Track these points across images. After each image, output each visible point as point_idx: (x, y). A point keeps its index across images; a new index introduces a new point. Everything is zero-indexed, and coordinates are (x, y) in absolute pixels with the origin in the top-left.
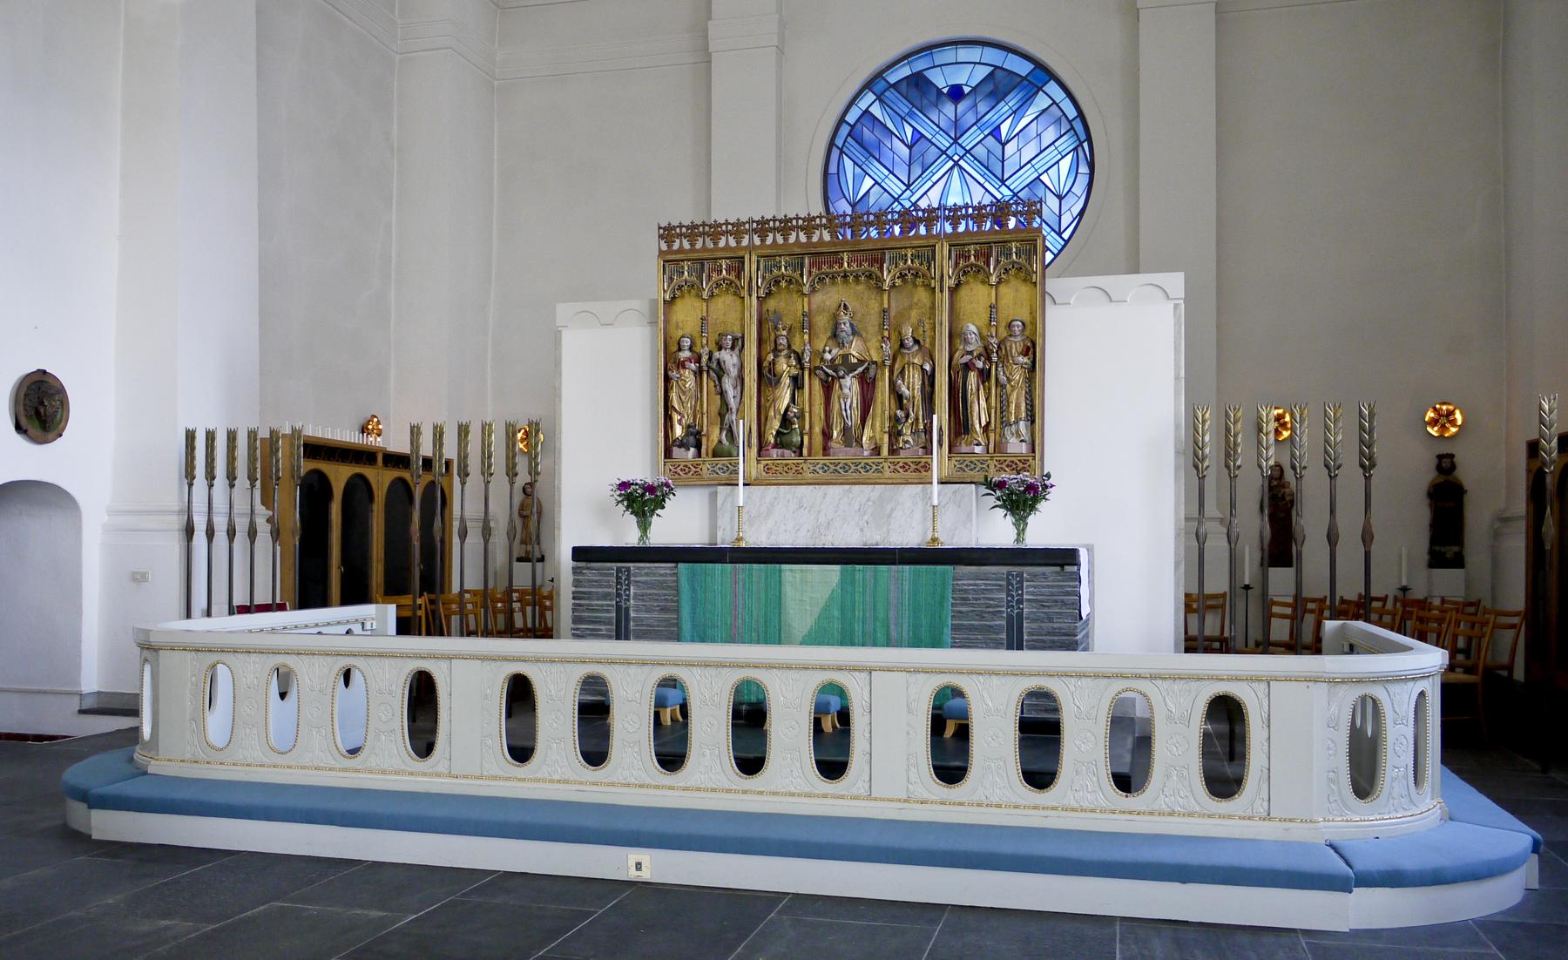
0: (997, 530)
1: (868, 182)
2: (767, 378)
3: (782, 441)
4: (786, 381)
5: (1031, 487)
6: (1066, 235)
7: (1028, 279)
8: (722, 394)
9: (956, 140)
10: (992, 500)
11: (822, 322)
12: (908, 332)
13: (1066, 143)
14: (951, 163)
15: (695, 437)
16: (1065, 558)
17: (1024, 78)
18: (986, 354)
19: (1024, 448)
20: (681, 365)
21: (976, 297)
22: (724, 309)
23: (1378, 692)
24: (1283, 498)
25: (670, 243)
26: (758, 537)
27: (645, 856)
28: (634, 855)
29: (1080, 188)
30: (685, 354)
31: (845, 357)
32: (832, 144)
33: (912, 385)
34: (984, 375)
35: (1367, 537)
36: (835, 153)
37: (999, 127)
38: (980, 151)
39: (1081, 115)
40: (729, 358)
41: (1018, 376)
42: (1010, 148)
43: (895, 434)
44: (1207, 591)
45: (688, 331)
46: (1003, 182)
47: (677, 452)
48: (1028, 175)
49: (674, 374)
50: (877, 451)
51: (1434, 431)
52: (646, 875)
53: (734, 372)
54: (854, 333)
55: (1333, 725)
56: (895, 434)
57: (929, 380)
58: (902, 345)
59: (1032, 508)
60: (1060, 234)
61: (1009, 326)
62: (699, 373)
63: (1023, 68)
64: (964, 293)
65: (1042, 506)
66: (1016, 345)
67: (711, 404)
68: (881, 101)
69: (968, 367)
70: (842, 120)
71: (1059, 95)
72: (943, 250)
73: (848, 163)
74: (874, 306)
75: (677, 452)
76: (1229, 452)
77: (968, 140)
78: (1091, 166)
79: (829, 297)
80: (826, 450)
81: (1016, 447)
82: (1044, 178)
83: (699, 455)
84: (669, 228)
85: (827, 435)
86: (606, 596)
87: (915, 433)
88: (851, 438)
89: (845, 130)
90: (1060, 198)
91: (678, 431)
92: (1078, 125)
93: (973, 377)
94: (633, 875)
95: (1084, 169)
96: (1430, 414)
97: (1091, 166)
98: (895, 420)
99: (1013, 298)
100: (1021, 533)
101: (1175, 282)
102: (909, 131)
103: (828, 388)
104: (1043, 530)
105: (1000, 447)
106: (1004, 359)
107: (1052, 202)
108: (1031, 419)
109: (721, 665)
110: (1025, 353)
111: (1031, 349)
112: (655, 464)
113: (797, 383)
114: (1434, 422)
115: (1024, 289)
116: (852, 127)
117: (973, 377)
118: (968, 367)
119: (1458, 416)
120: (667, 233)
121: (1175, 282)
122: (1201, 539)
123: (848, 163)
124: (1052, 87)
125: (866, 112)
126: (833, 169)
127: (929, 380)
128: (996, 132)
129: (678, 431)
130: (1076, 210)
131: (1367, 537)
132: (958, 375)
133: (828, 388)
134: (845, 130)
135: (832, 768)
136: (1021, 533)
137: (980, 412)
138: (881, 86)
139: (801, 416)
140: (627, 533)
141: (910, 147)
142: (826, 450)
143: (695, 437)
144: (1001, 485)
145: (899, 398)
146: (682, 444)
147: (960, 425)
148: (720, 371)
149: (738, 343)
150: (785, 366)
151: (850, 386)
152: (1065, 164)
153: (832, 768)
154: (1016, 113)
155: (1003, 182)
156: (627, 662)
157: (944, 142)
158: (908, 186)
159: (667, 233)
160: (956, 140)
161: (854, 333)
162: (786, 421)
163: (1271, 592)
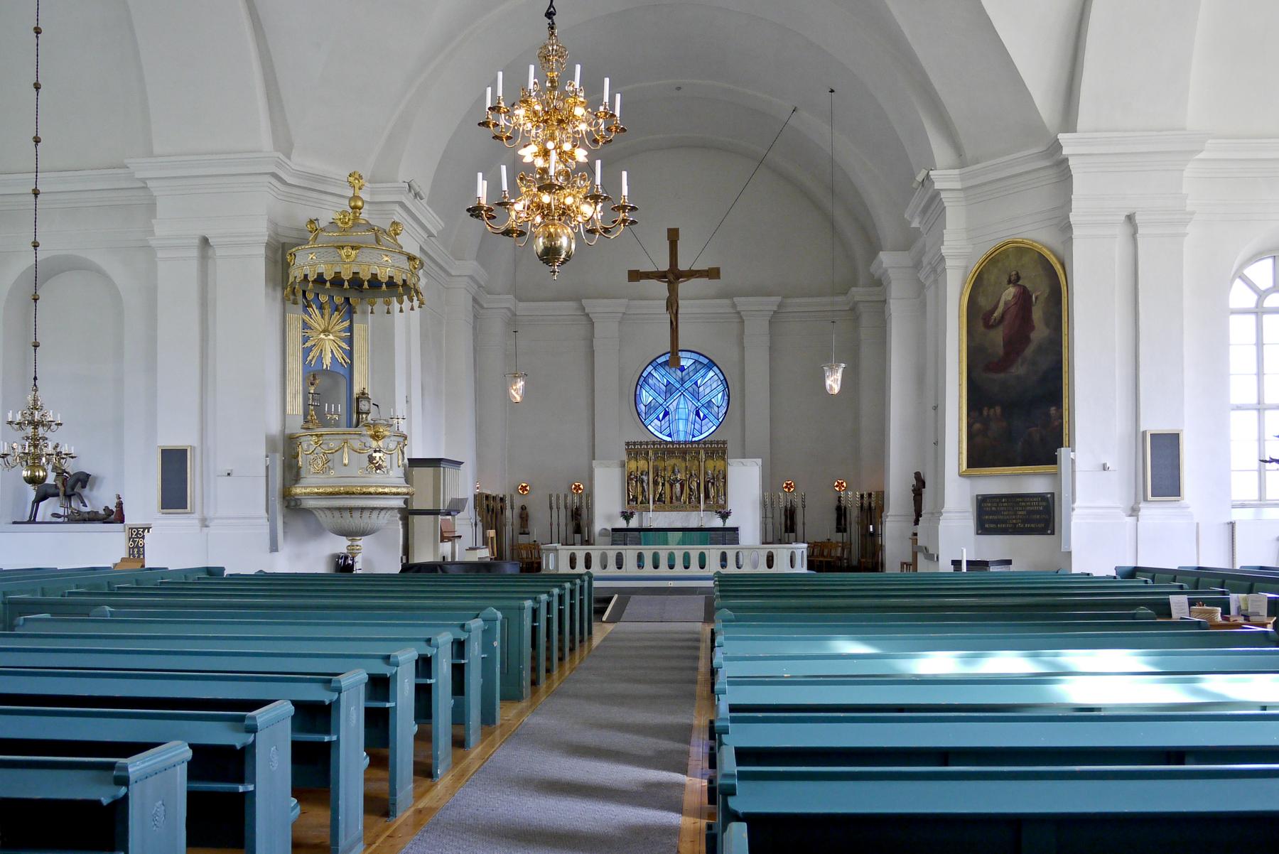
0: (717, 522)
1: (651, 398)
2: (656, 483)
3: (659, 500)
4: (661, 484)
5: (727, 513)
6: (720, 420)
7: (724, 459)
8: (643, 487)
9: (682, 385)
10: (717, 516)
11: (669, 468)
12: (693, 472)
13: (721, 388)
14: (680, 393)
15: (635, 498)
16: (736, 530)
17: (705, 365)
18: (714, 479)
19: (723, 502)
20: (632, 479)
21: (710, 464)
22: (642, 464)
23: (795, 550)
24: (620, 838)
25: (628, 447)
26: (655, 525)
27: (671, 582)
28: (670, 582)
29: (725, 404)
30: (632, 477)
31: (676, 478)
32: (637, 384)
33: (694, 486)
34: (713, 484)
35: (804, 524)
36: (639, 387)
37: (697, 381)
38: (691, 389)
39: (725, 379)
40: (645, 478)
41: (721, 484)
42: (701, 389)
43: (690, 499)
44: (1267, 472)
45: (633, 470)
46: (699, 401)
47: (630, 502)
48: (707, 399)
49: (630, 482)
50: (685, 503)
51: (837, 489)
52: (672, 586)
53: (646, 481)
54: (679, 472)
55: (787, 556)
56: (690, 499)
57: (699, 485)
58: (691, 475)
59: (727, 518)
60: (718, 420)
61: (719, 472)
62: (636, 482)
63: (706, 361)
64: (707, 462)
65: (729, 517)
66: (721, 477)
67: (639, 489)
68: (655, 370)
69: (709, 482)
70: (641, 375)
71: (718, 371)
72: (702, 452)
73: (644, 391)
74: (684, 465)
75: (630, 502)
76: (772, 504)
77: (687, 385)
78: (729, 396)
79: (673, 461)
80: (671, 502)
81: (721, 502)
82: (713, 400)
83: (637, 503)
84: (628, 442)
85: (671, 498)
86: (620, 541)
87: (695, 498)
88: (678, 499)
89: (642, 379)
90: (718, 407)
91: (631, 497)
92: (724, 382)
93: (710, 484)
94: (670, 585)
95: (726, 398)
96: (836, 484)
97: (729, 396)
98: (690, 495)
99: (719, 464)
100: (724, 523)
101: (759, 461)
102: (665, 381)
103: (671, 486)
104: (730, 523)
105: (717, 502)
106: (718, 479)
107: (716, 409)
108: (725, 495)
109: (681, 549)
110: (723, 478)
111: (725, 478)
112: (623, 504)
113: (663, 485)
114: (837, 486)
115: (723, 462)
116: (645, 378)
117: (710, 484)
118: (709, 482)
119: (845, 484)
120: (628, 444)
121: (759, 461)
122: (766, 525)
123: (644, 391)
124: (715, 368)
125: (650, 373)
126: (638, 393)
127: (699, 485)
128: (696, 383)
129: (631, 497)
130: (724, 412)
131: (804, 524)
132: (706, 483)
133: (671, 486)
134: (642, 379)
135: (702, 567)
136: (724, 523)
137: (712, 492)
138: (654, 364)
139: (665, 493)
140: (621, 524)
141: (666, 387)
142: (671, 502)
143: (635, 498)
144: (720, 512)
145: (691, 489)
146: (632, 500)
147: (707, 496)
148: (642, 481)
149: (648, 473)
150: (660, 480)
151: (678, 485)
152: (720, 395)
153: (702, 567)
154: (703, 376)
155: (699, 401)
156: (693, 549)
157: (678, 385)
158: (665, 400)
159: (628, 444)
160: (682, 385)
161: (679, 472)
162: (661, 495)
163: (416, 517)
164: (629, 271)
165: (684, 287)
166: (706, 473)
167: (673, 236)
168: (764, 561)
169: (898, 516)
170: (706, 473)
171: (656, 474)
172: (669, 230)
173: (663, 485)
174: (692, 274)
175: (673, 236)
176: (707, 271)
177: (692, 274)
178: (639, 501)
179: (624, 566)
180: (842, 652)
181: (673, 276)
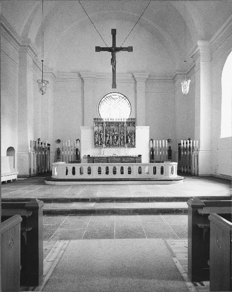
2: (106, 136)
15: (98, 142)
40: (102, 134)
43: (120, 143)
105: (132, 144)
111: (135, 134)
113: (109, 137)
135: (89, 173)
143: (98, 142)
150: (108, 135)
153: (89, 173)
159: (95, 119)
164: (96, 51)
165: (118, 55)
166: (127, 132)
167: (114, 32)
168: (70, 171)
169: (82, 88)
170: (127, 132)
171: (106, 132)
172: (132, 48)
173: (109, 137)
174: (121, 49)
175: (114, 32)
176: (127, 48)
177: (121, 49)
178: (99, 143)
179: (132, 172)
180: (187, 224)
181: (114, 50)
